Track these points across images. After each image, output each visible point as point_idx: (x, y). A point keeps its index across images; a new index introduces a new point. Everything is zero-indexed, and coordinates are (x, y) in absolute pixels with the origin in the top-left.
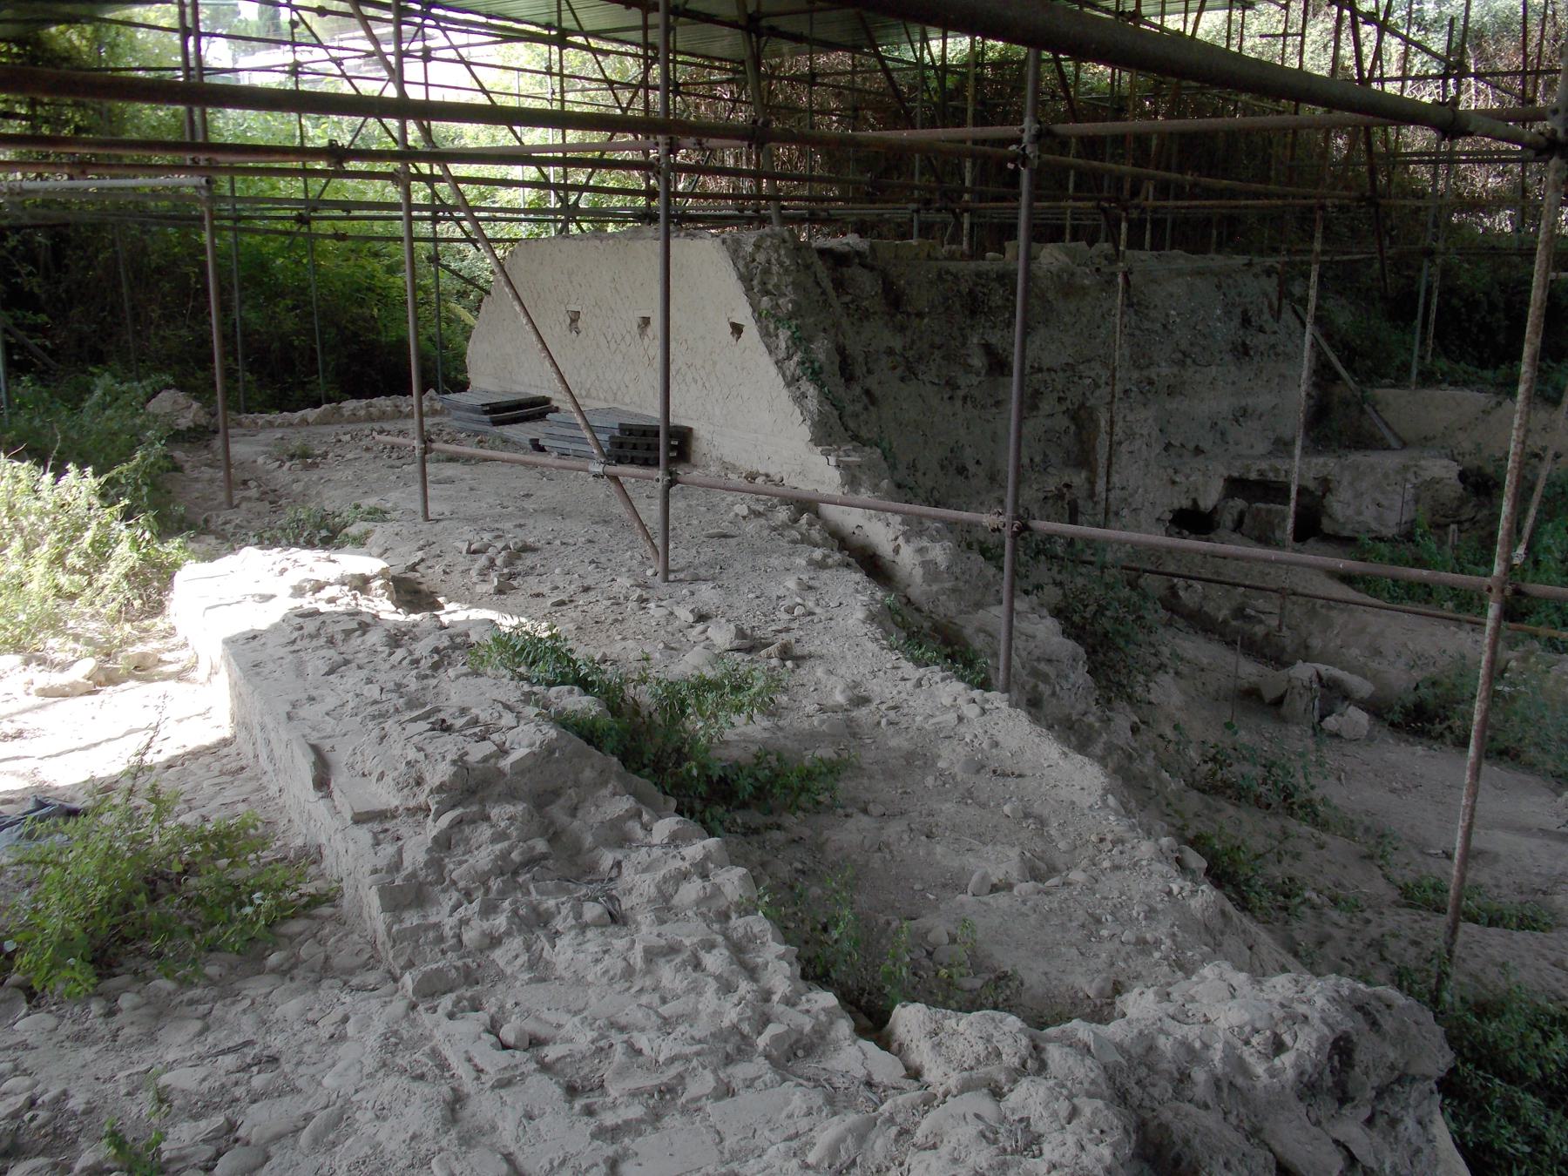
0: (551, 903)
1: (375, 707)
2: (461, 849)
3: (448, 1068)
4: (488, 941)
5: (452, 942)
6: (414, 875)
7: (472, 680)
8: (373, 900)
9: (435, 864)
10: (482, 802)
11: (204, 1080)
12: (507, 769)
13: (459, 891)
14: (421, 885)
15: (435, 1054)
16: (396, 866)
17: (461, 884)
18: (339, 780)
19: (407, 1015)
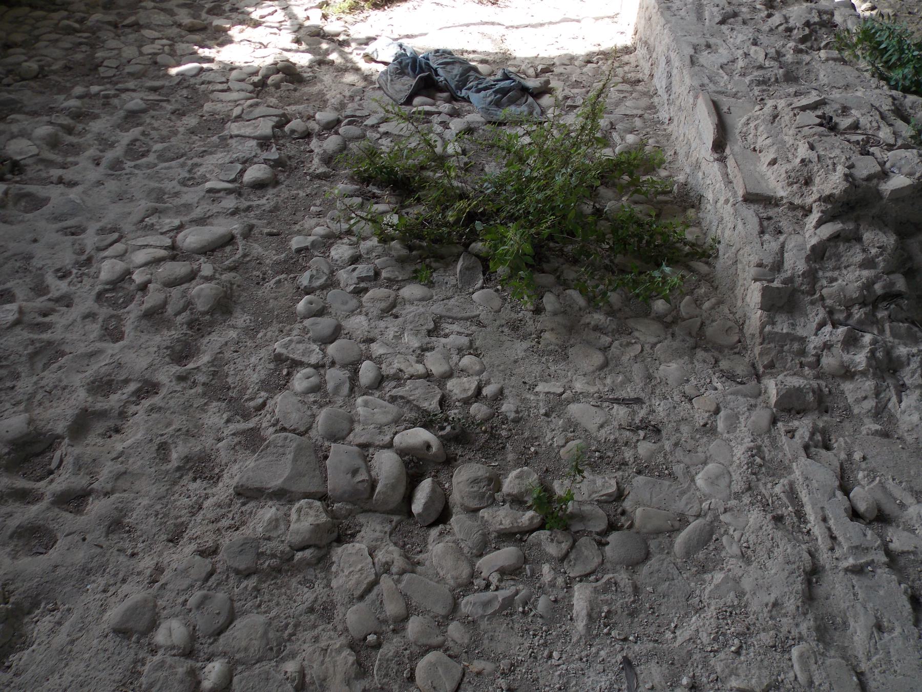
0: (902, 351)
1: (761, 72)
2: (831, 264)
3: (806, 522)
4: (843, 372)
5: (811, 359)
6: (791, 280)
7: (839, 67)
8: (754, 294)
9: (811, 276)
10: (857, 220)
11: (602, 426)
12: (886, 194)
13: (825, 307)
14: (795, 291)
15: (792, 493)
16: (778, 266)
17: (829, 302)
18: (733, 149)
19: (769, 431)
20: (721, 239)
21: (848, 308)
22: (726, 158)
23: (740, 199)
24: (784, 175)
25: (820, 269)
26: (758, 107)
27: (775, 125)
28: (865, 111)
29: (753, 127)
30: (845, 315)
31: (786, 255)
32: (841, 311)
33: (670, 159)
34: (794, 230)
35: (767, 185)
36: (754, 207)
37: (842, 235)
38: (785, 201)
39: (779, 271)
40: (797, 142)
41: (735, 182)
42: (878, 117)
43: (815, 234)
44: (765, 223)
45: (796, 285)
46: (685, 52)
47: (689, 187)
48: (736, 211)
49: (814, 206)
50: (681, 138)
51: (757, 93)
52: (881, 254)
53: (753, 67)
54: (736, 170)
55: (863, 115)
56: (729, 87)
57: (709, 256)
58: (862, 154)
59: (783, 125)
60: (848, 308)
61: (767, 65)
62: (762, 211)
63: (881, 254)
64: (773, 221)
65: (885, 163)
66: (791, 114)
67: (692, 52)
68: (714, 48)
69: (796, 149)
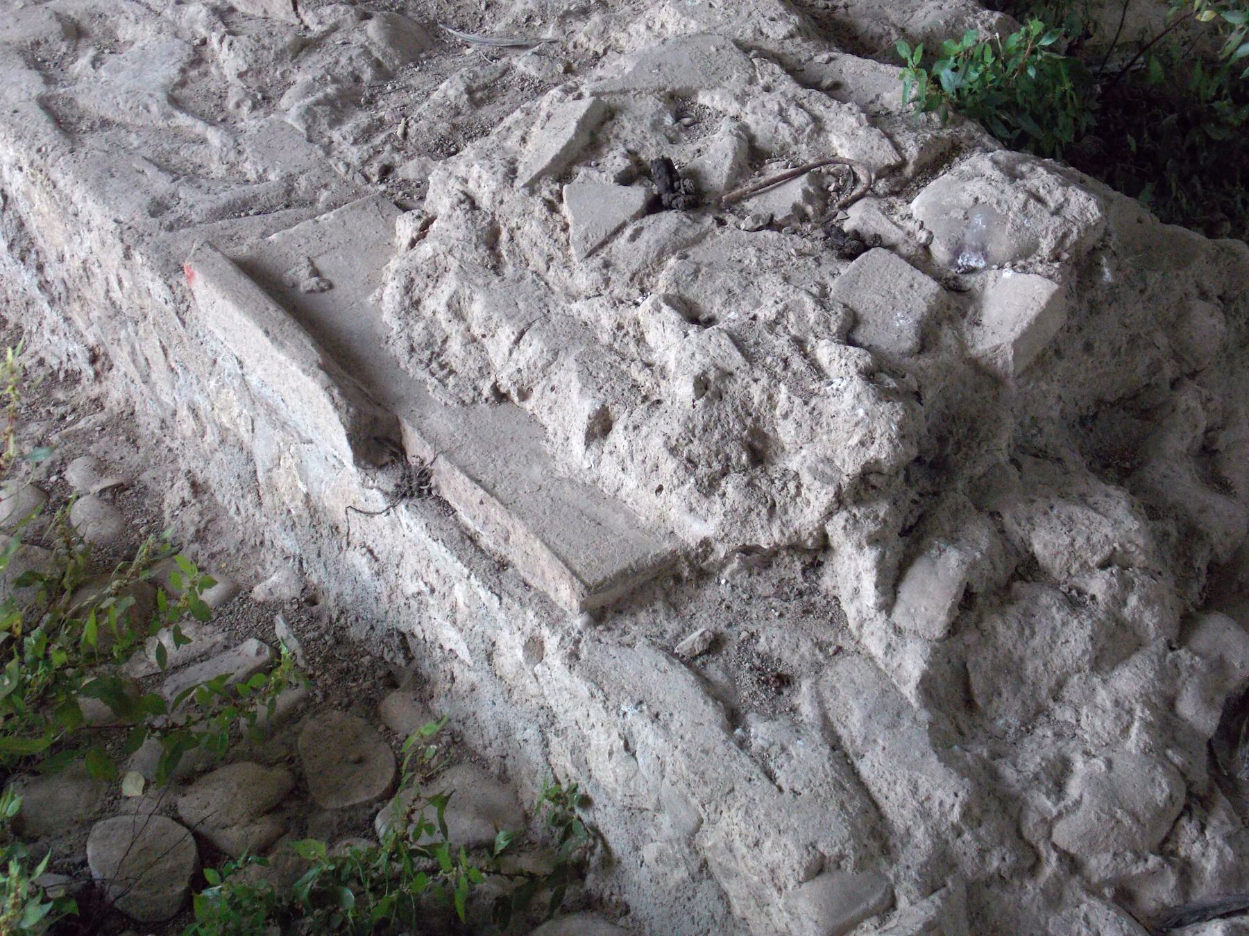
12: (1006, 359)
13: (1094, 891)
17: (1099, 865)
20: (585, 788)
21: (1165, 848)
22: (425, 475)
23: (579, 621)
24: (669, 466)
25: (996, 755)
26: (405, 227)
27: (509, 270)
28: (736, 80)
29: (443, 316)
30: (1172, 879)
31: (864, 768)
32: (1151, 875)
33: (191, 517)
34: (820, 645)
35: (631, 517)
36: (639, 625)
37: (979, 588)
38: (721, 550)
39: (887, 850)
40: (630, 313)
41: (515, 557)
42: (788, 86)
43: (898, 631)
44: (715, 671)
45: (968, 867)
46: (14, 96)
47: (328, 603)
48: (594, 677)
49: (835, 530)
50: (187, 426)
51: (355, 154)
52: (1127, 585)
53: (279, 57)
54: (495, 512)
55: (742, 98)
56: (250, 169)
57: (580, 870)
58: (852, 257)
59: (537, 262)
60: (1165, 848)
61: (316, 29)
62: (672, 627)
63: (1127, 585)
64: (732, 649)
65: (926, 247)
66: (539, 209)
67: (32, 83)
68: (96, 30)
69: (640, 340)
